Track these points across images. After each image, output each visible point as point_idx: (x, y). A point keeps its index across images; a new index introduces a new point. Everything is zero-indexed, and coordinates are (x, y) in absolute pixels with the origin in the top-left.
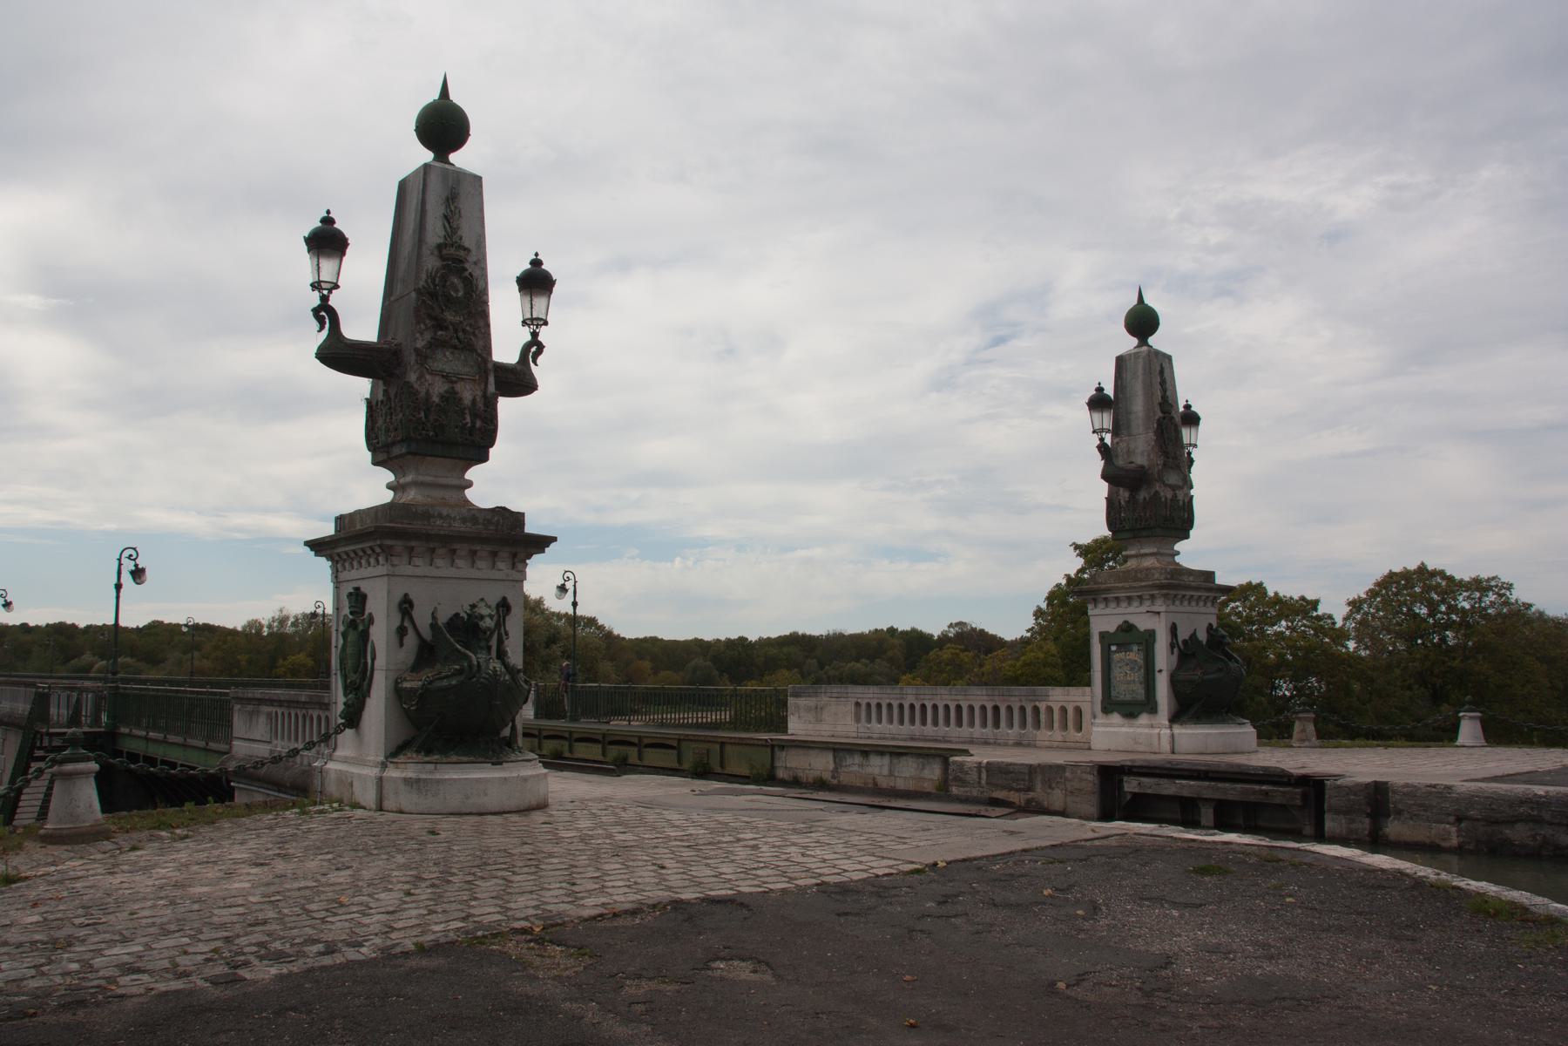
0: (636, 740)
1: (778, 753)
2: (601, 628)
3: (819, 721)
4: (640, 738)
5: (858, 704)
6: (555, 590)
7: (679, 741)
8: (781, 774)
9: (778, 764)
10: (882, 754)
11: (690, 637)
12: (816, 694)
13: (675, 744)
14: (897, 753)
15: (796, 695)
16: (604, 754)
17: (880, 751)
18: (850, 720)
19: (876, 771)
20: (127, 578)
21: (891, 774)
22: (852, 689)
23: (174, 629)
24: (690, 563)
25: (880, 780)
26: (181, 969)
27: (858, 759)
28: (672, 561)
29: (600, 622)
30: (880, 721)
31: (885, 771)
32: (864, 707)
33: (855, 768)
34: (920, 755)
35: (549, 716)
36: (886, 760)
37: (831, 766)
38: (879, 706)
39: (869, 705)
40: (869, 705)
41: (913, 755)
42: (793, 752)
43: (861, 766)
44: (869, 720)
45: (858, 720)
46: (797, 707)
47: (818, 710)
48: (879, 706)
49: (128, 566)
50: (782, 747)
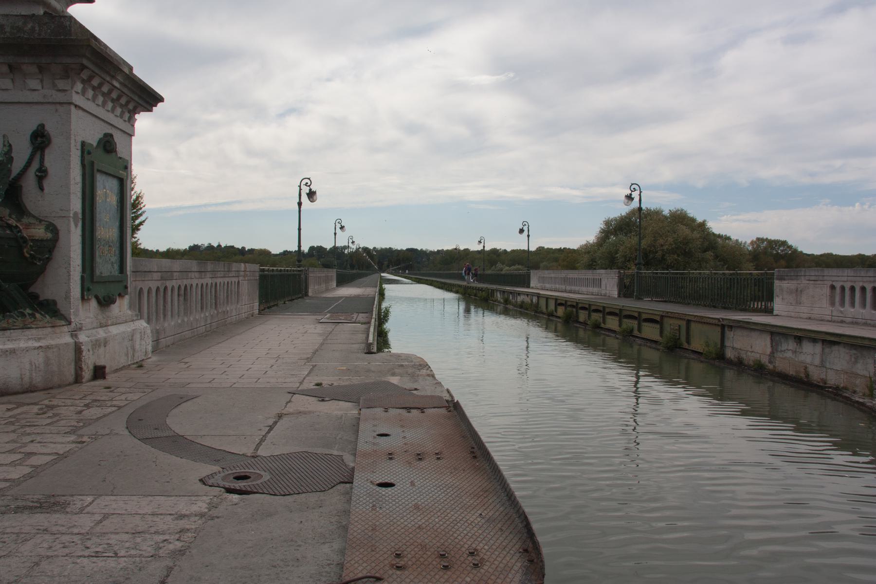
0: (636, 315)
1: (729, 334)
2: (790, 247)
3: (799, 303)
4: (640, 313)
5: (833, 287)
6: (623, 198)
7: (662, 317)
8: (730, 354)
9: (728, 343)
10: (814, 341)
11: (856, 253)
12: (797, 277)
13: (658, 318)
14: (830, 341)
15: (781, 278)
16: (620, 325)
17: (814, 337)
18: (825, 303)
19: (808, 359)
20: (305, 198)
21: (822, 365)
22: (828, 272)
23: (550, 251)
24: (866, 207)
25: (811, 369)
26: (867, 392)
27: (791, 345)
28: (853, 205)
29: (790, 243)
30: (853, 304)
31: (817, 361)
32: (838, 290)
33: (789, 354)
34: (853, 346)
35: (625, 296)
36: (818, 347)
37: (769, 350)
38: (853, 289)
39: (843, 288)
40: (843, 288)
41: (846, 345)
42: (739, 332)
43: (795, 352)
44: (842, 304)
45: (833, 304)
46: (782, 290)
47: (798, 292)
48: (853, 289)
49: (305, 190)
50: (731, 327)
